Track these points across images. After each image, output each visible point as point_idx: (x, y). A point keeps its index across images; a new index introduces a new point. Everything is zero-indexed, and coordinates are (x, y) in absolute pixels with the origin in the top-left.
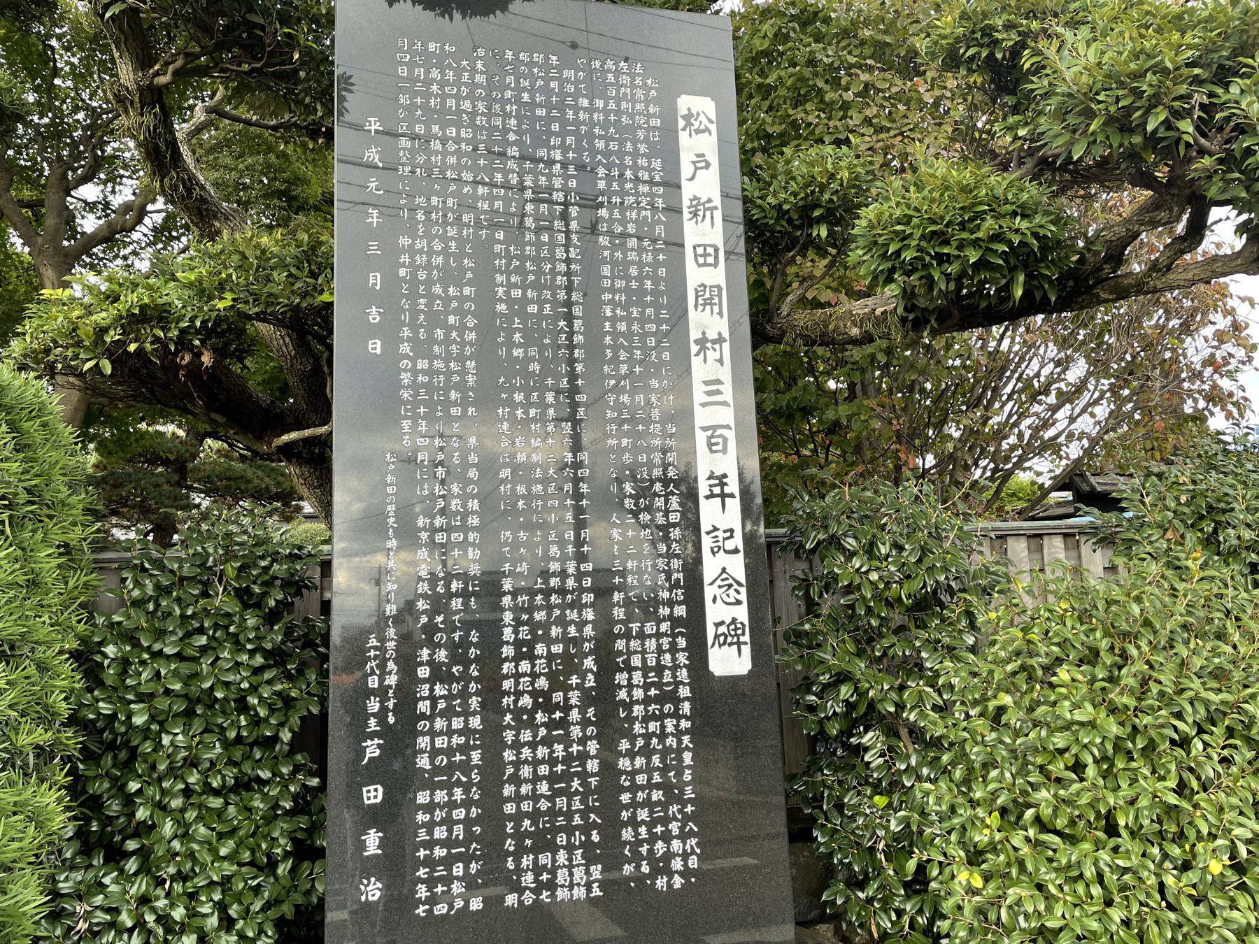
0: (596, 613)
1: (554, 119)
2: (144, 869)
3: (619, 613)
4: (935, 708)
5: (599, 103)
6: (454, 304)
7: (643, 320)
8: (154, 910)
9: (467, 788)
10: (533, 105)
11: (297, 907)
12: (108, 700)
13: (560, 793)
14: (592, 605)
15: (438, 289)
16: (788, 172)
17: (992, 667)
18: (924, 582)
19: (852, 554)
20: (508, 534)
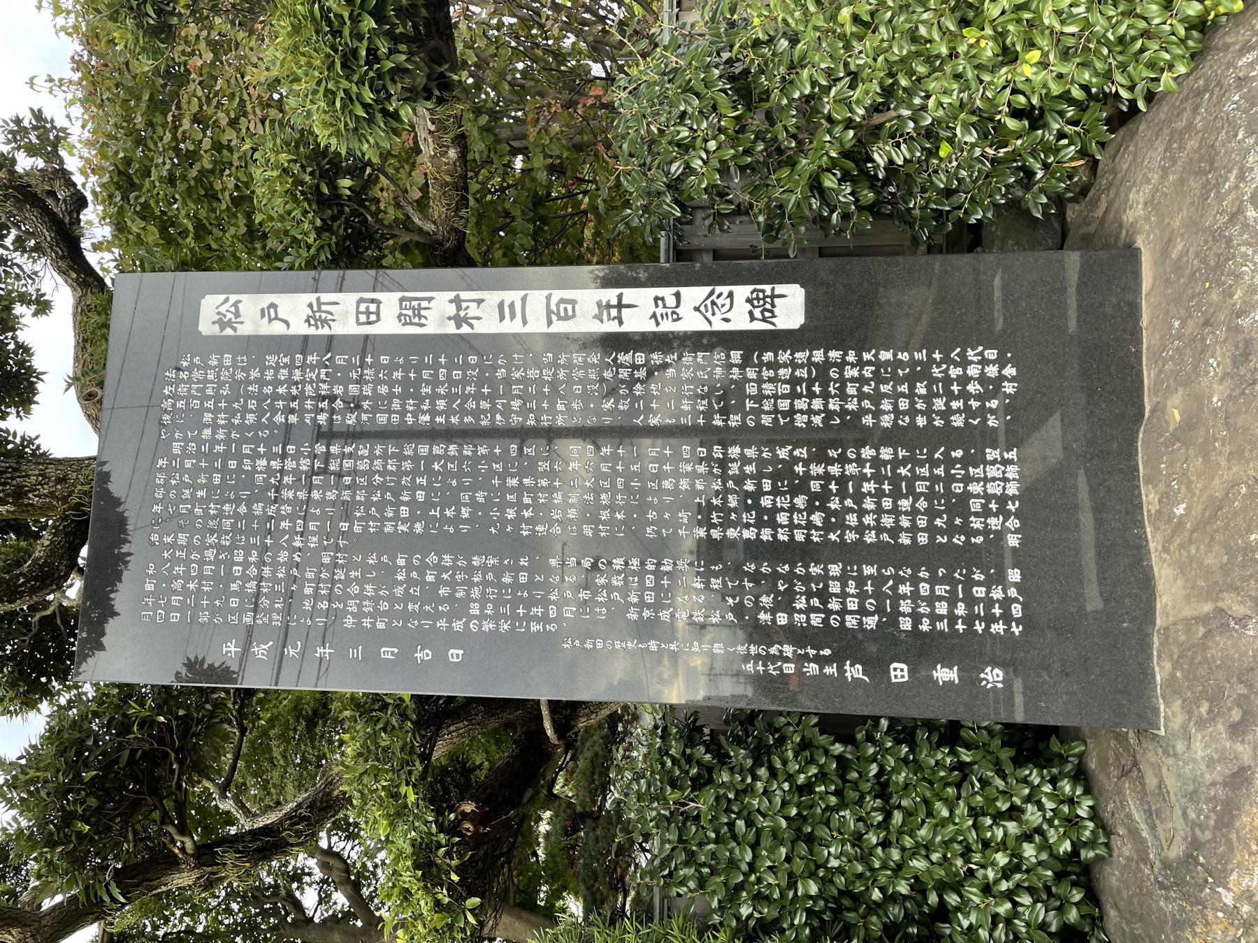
0: (733, 443)
1: (224, 465)
2: (957, 888)
3: (735, 420)
4: (852, 87)
5: (208, 417)
6: (414, 575)
7: (435, 382)
8: (997, 882)
9: (899, 580)
10: (209, 486)
11: (1004, 744)
12: (793, 915)
13: (911, 487)
14: (725, 447)
15: (399, 591)
16: (282, 218)
17: (810, 27)
18: (720, 91)
19: (688, 167)
20: (649, 530)
